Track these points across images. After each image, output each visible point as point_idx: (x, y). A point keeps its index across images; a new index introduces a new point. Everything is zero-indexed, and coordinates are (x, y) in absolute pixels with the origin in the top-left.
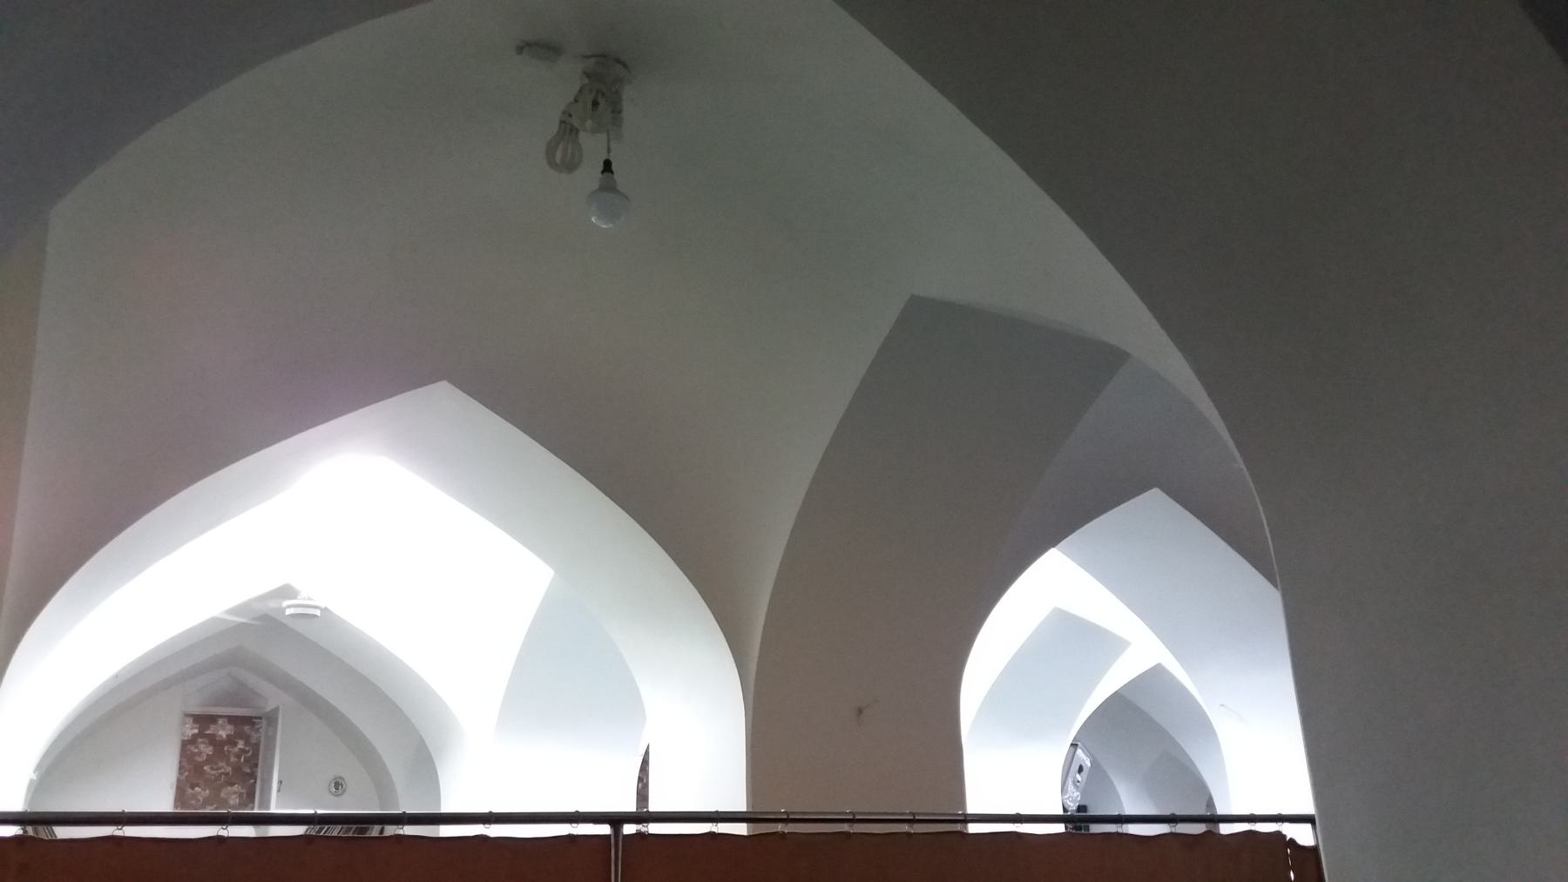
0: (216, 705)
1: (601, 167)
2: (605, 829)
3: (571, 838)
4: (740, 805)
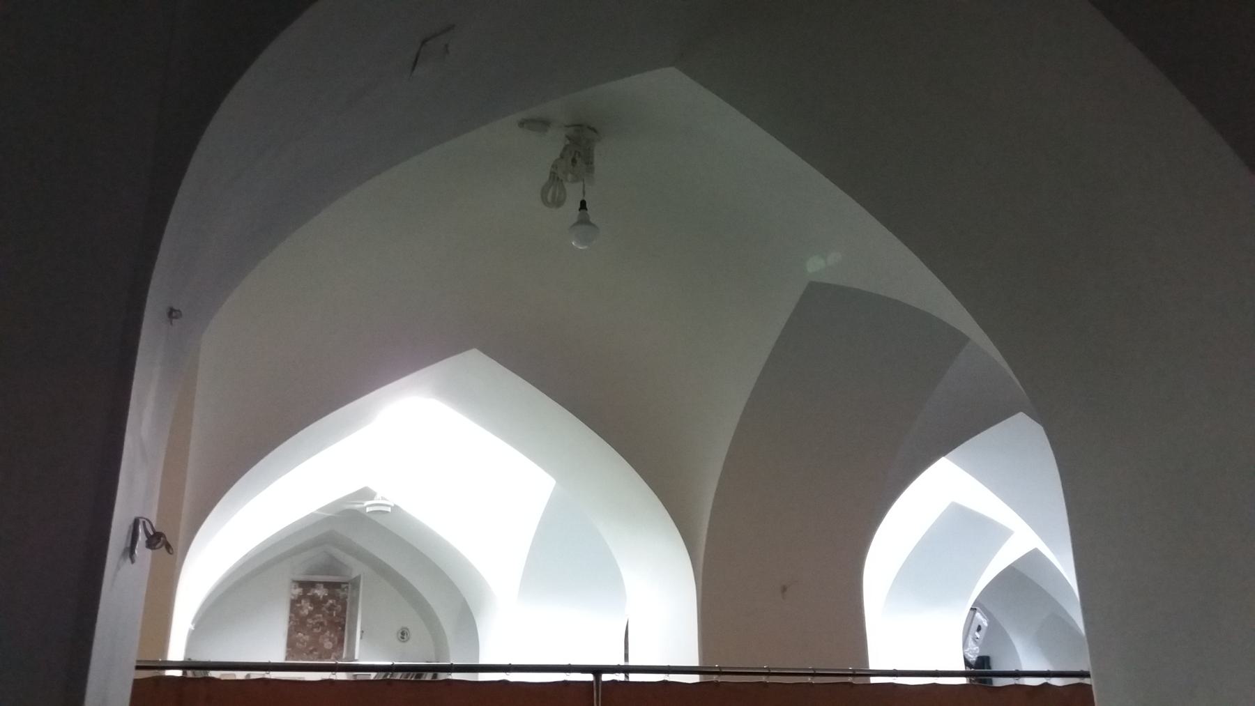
0: (313, 574)
1: (579, 206)
2: (589, 677)
3: (565, 683)
4: (694, 661)
